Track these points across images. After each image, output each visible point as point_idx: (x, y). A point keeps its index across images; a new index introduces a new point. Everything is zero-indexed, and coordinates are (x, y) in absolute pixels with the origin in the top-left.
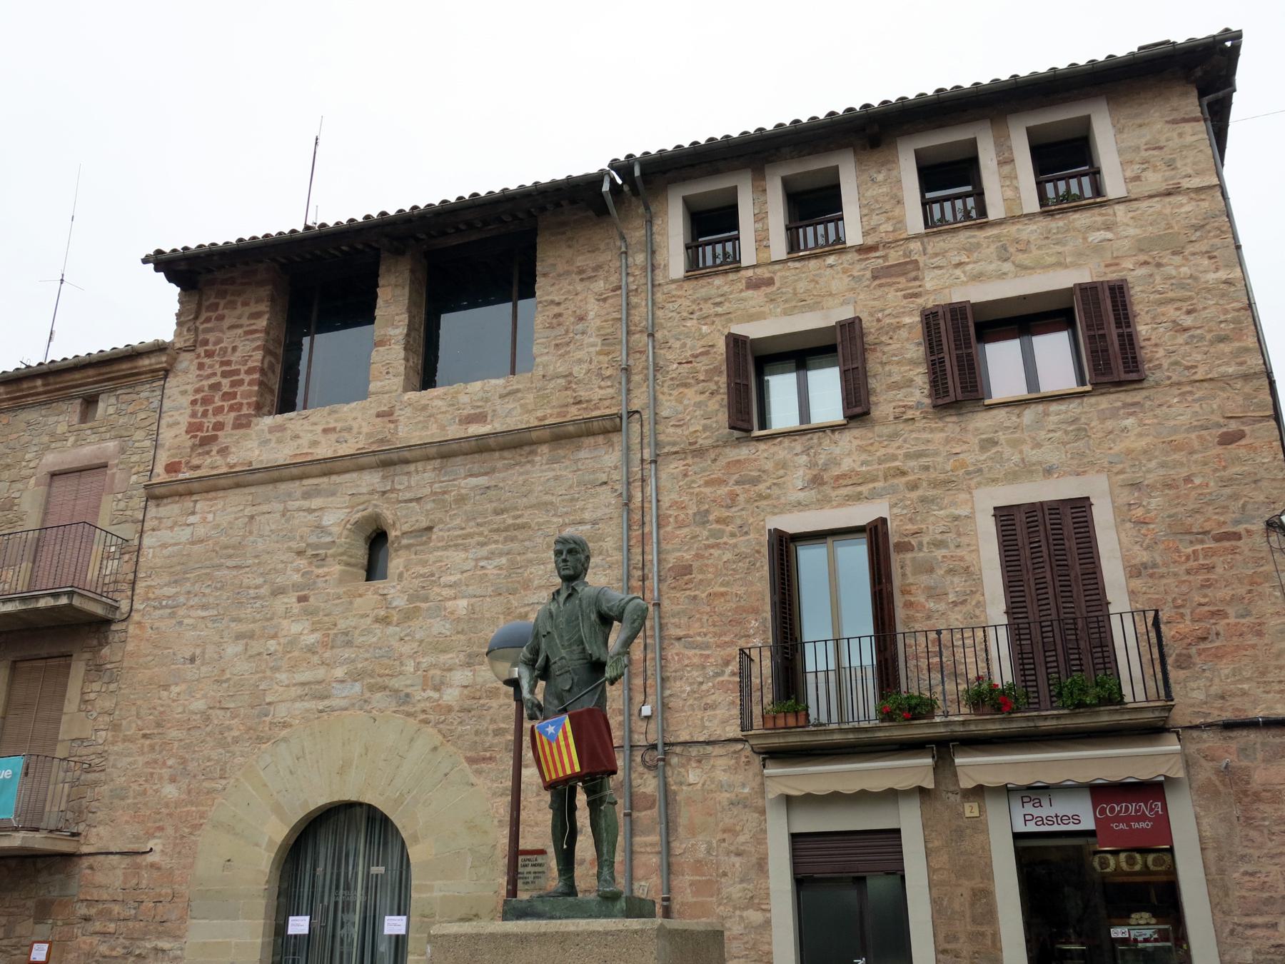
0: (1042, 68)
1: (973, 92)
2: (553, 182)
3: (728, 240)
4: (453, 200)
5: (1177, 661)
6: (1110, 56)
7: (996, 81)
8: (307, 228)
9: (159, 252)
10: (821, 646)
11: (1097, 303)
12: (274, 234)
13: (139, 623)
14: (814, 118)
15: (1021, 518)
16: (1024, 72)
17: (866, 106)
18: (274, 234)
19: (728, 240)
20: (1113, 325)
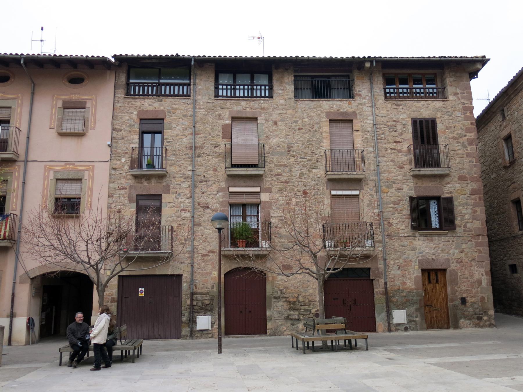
0: (283, 56)
1: (351, 60)
2: (280, 57)
3: (183, 85)
4: (217, 56)
5: (20, 280)
6: (331, 57)
7: (286, 57)
8: (177, 55)
9: (115, 55)
10: (157, 157)
11: (422, 124)
12: (212, 56)
13: (117, 100)
14: (297, 56)
15: (424, 122)
16: (278, 56)
17: (220, 56)
18: (212, 56)
19: (183, 85)
20: (73, 214)
